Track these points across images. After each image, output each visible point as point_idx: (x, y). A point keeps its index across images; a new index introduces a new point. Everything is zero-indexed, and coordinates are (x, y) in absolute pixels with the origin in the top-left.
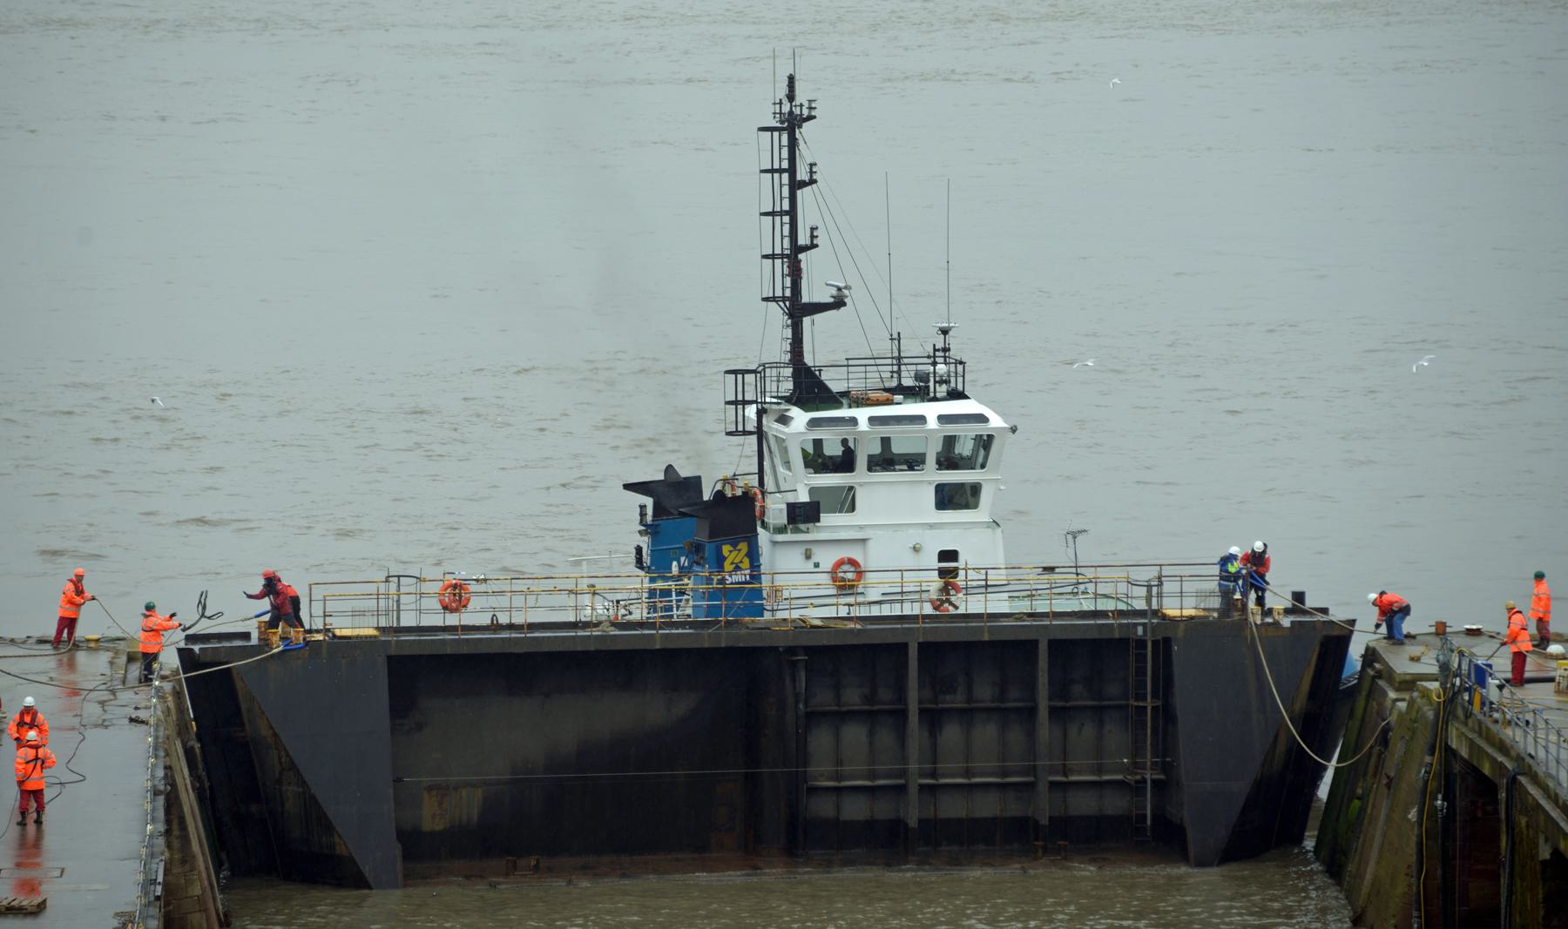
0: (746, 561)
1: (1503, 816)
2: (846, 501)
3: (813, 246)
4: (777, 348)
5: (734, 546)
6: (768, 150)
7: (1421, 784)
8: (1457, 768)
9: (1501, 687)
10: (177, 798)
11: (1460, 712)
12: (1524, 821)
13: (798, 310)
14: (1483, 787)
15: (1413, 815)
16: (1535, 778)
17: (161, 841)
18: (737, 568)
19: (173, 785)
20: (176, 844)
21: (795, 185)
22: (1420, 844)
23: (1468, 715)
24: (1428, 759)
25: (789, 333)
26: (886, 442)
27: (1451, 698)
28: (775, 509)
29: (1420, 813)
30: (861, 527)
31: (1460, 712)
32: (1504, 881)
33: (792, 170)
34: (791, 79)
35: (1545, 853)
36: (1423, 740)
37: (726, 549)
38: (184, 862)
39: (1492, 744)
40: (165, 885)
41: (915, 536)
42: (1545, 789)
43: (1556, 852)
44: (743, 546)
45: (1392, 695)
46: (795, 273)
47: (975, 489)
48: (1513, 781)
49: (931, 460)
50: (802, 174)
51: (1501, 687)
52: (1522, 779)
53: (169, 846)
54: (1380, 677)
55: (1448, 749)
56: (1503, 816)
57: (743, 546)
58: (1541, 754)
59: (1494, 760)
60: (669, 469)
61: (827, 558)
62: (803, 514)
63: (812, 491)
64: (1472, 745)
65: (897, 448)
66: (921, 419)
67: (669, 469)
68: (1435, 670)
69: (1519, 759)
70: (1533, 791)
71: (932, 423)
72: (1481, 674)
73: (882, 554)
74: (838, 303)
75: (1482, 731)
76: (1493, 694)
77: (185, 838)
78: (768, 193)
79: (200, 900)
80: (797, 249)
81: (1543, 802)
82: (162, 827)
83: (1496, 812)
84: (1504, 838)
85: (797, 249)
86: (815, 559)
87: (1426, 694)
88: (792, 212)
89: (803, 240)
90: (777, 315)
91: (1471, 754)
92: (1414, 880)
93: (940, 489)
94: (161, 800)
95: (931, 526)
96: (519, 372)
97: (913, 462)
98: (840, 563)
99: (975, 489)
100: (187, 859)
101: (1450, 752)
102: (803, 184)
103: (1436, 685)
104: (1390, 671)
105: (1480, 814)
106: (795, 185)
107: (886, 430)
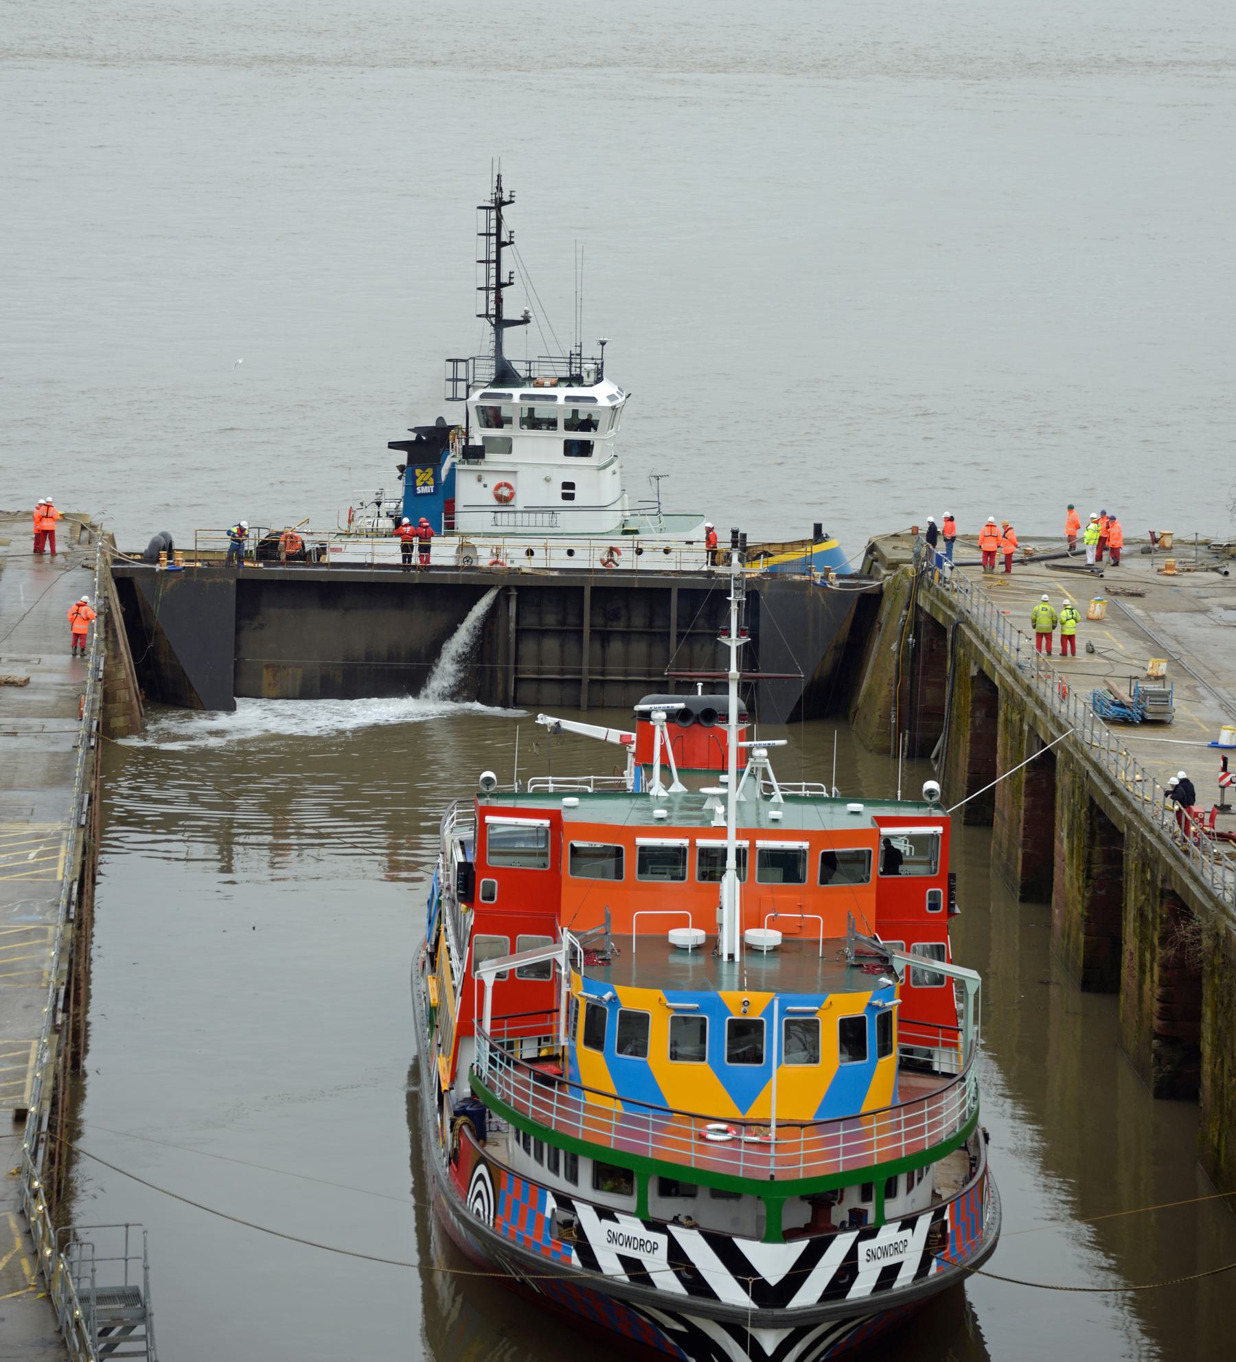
0: (432, 480)
1: (949, 648)
2: (506, 446)
3: (511, 284)
4: (488, 348)
5: (424, 469)
6: (482, 221)
7: (899, 628)
8: (922, 618)
9: (952, 568)
10: (112, 617)
11: (926, 584)
12: (962, 652)
13: (500, 323)
14: (939, 630)
15: (894, 647)
17: (102, 646)
18: (425, 484)
19: (109, 608)
20: (110, 646)
21: (500, 244)
22: (898, 665)
23: (931, 585)
24: (904, 612)
25: (493, 338)
26: (531, 410)
27: (920, 576)
29: (899, 645)
30: (515, 464)
31: (926, 584)
32: (948, 690)
33: (498, 235)
34: (499, 176)
35: (974, 672)
36: (902, 601)
37: (418, 472)
38: (115, 657)
39: (945, 604)
40: (105, 671)
41: (547, 472)
42: (976, 632)
43: (981, 671)
44: (430, 471)
45: (884, 572)
46: (499, 301)
48: (957, 627)
49: (561, 424)
50: (504, 238)
51: (952, 568)
52: (962, 626)
53: (107, 647)
54: (876, 560)
55: (917, 606)
56: (949, 648)
57: (430, 471)
58: (975, 611)
59: (945, 614)
60: (440, 419)
61: (492, 481)
63: (484, 439)
64: (932, 603)
65: (537, 415)
67: (440, 419)
68: (910, 556)
69: (961, 613)
70: (969, 633)
71: (561, 401)
74: (526, 321)
75: (939, 595)
76: (947, 573)
77: (116, 642)
78: (482, 248)
79: (125, 682)
80: (500, 285)
81: (975, 641)
82: (103, 636)
83: (945, 646)
84: (949, 662)
85: (500, 285)
86: (484, 482)
87: (905, 572)
88: (498, 261)
89: (504, 279)
90: (487, 327)
91: (931, 610)
92: (893, 688)
93: (566, 442)
94: (102, 618)
95: (560, 466)
97: (552, 424)
98: (499, 487)
100: (116, 655)
101: (918, 609)
102: (505, 244)
104: (883, 556)
105: (935, 647)
106: (500, 244)
107: (532, 404)
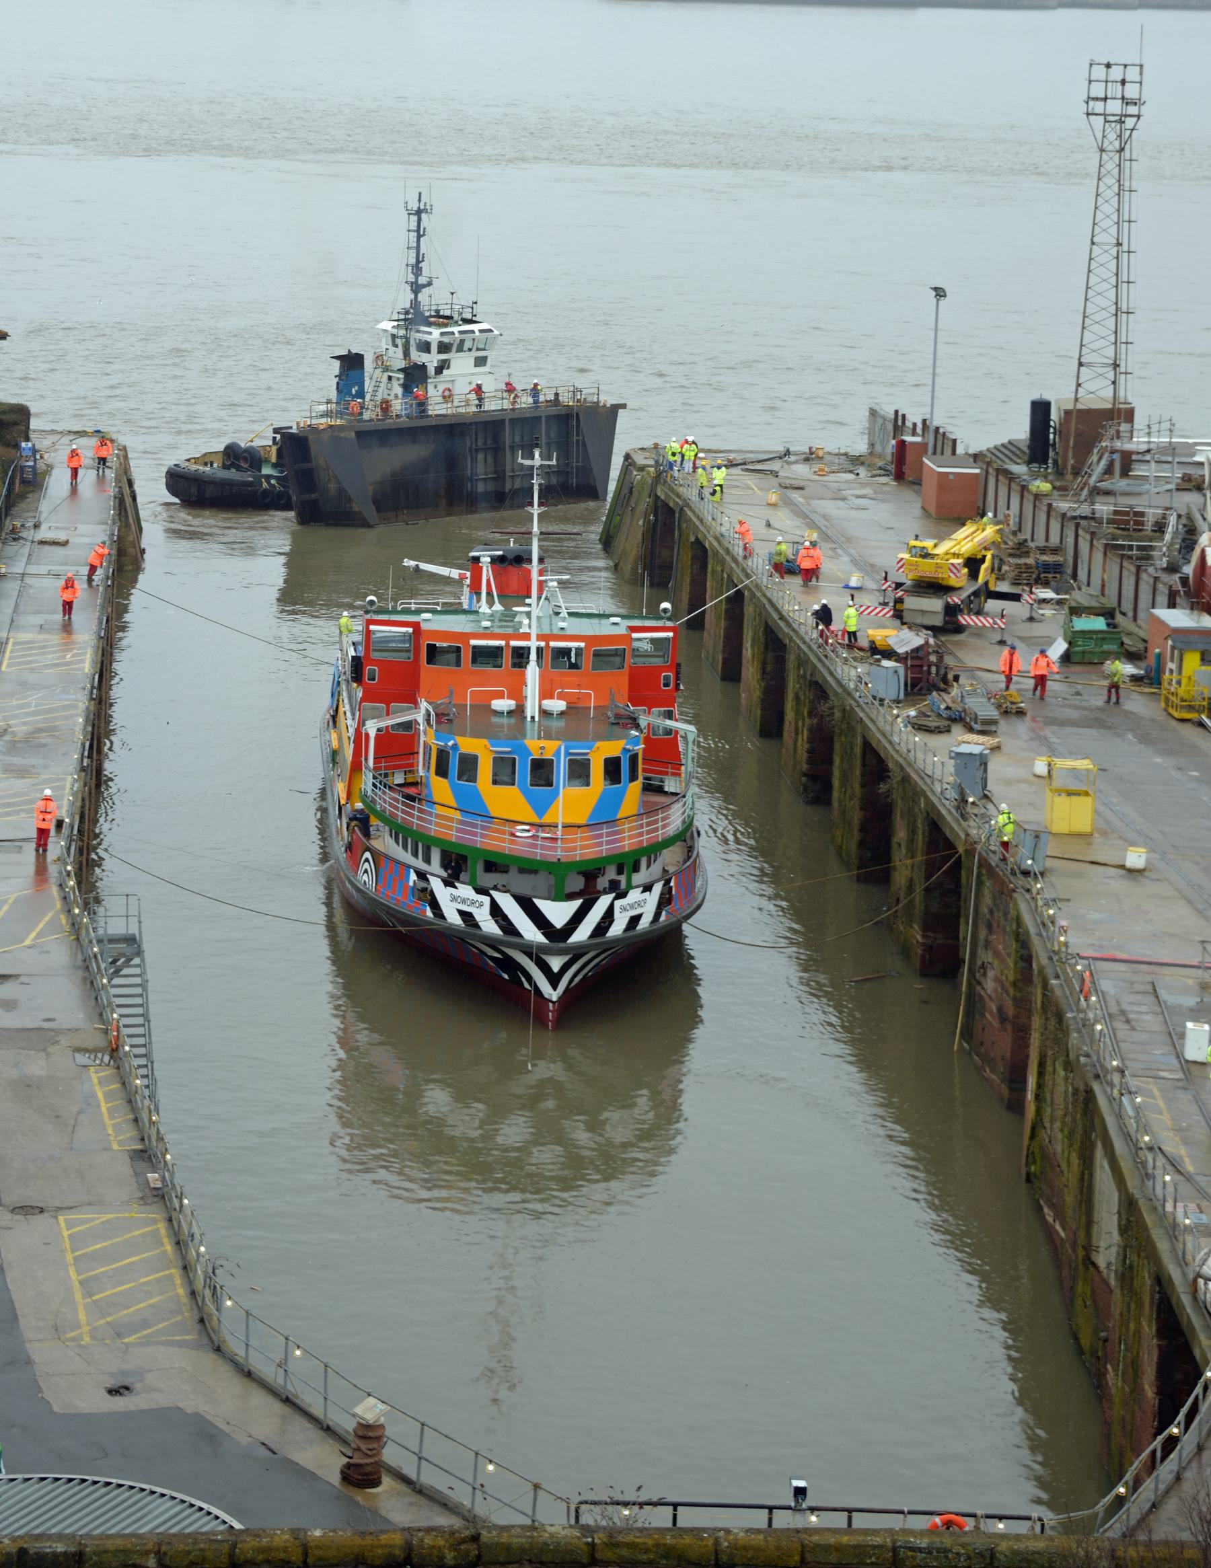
15: (641, 522)
16: (690, 508)
23: (665, 482)
27: (659, 475)
28: (431, 370)
35: (692, 539)
36: (646, 493)
42: (694, 512)
47: (486, 358)
48: (682, 509)
62: (439, 370)
66: (473, 332)
70: (689, 513)
72: (671, 465)
73: (459, 388)
77: (127, 517)
87: (649, 473)
93: (477, 359)
96: (335, 722)
99: (486, 358)
101: (657, 497)
103: (652, 469)
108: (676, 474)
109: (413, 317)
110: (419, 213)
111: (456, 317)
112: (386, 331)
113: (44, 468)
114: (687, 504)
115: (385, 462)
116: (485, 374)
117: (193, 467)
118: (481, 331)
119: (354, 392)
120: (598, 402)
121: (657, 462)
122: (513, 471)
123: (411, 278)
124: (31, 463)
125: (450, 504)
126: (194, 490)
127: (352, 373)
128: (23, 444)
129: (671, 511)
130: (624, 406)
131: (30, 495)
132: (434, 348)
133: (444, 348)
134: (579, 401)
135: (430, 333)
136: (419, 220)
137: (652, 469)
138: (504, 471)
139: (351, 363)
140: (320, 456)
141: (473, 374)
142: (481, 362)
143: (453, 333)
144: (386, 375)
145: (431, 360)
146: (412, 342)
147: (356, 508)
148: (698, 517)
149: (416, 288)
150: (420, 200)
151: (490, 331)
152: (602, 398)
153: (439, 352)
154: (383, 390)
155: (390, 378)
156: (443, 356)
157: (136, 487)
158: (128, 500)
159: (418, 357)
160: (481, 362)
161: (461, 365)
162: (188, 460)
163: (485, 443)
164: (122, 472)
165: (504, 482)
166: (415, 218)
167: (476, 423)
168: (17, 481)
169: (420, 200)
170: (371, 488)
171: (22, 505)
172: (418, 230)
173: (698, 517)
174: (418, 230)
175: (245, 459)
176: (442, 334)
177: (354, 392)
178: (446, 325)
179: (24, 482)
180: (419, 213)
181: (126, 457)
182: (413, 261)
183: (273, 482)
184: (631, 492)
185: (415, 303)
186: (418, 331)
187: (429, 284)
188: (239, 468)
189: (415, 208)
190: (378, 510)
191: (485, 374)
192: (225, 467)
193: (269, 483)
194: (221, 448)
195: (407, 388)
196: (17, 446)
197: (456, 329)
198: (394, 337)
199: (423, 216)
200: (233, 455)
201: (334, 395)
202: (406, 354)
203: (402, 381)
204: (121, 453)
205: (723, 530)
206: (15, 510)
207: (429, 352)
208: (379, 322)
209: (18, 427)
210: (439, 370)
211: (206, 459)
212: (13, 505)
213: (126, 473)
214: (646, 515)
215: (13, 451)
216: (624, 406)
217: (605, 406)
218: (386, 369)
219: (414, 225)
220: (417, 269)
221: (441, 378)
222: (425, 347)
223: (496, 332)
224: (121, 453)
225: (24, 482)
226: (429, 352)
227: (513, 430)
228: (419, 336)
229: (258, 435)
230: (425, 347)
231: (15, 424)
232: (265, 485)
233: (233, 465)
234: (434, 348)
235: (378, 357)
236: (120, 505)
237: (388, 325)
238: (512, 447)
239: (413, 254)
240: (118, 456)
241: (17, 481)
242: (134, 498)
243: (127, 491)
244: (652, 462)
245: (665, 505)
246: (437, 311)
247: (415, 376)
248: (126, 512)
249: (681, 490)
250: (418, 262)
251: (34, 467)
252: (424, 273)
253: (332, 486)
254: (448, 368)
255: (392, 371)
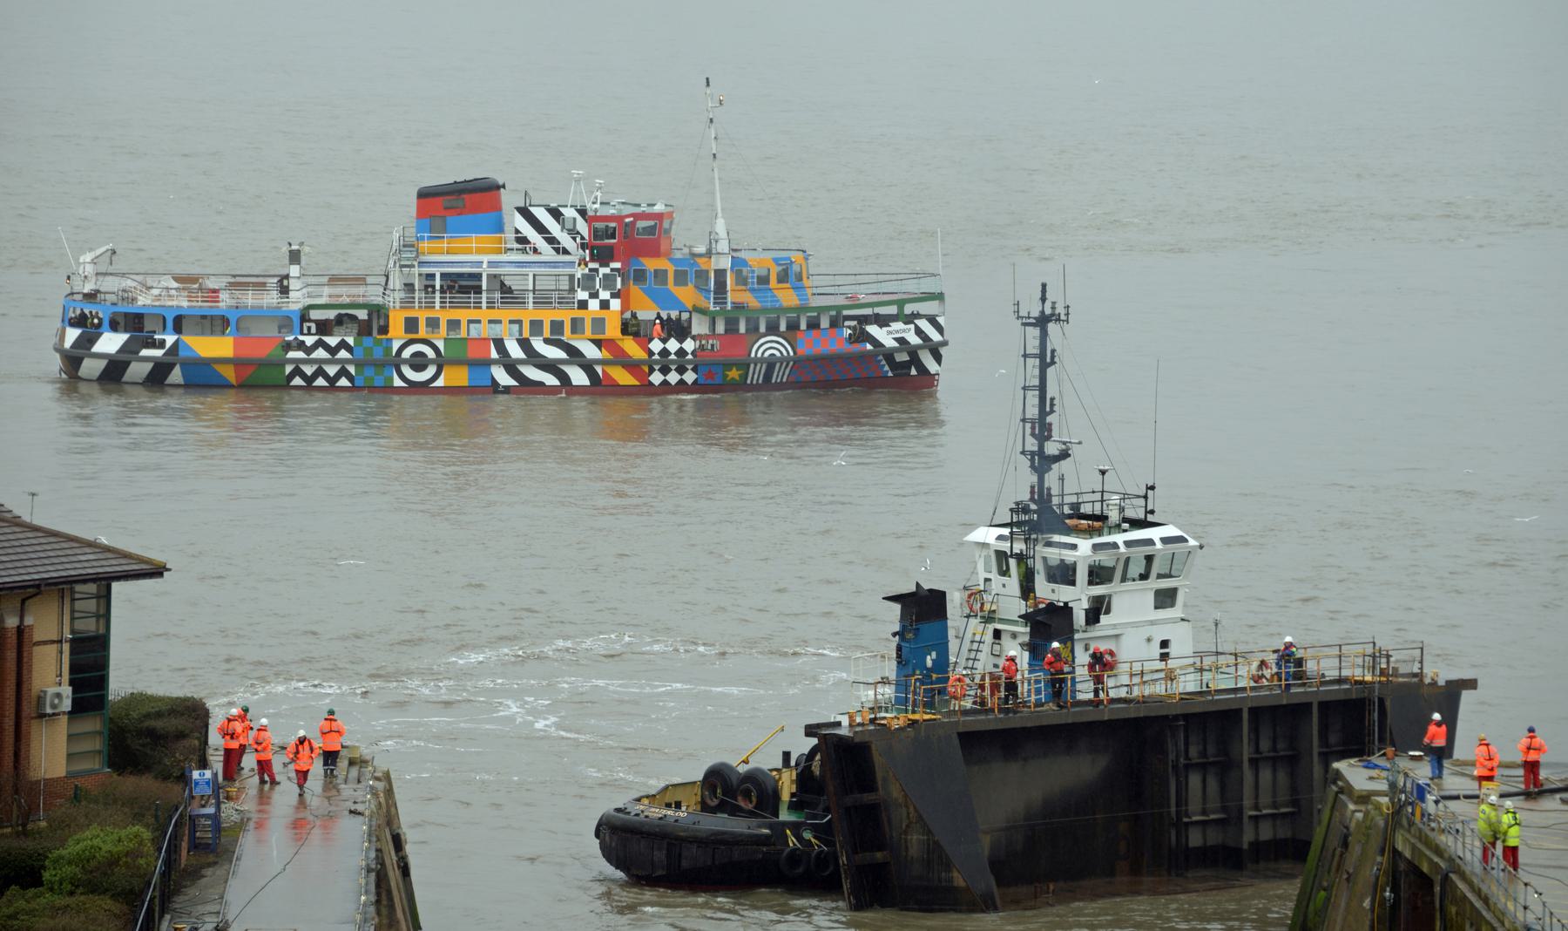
15: (1367, 903)
23: (1411, 824)
27: (1398, 810)
28: (1079, 617)
36: (1375, 843)
48: (1446, 878)
62: (1093, 616)
66: (1150, 542)
70: (1461, 885)
72: (1421, 792)
73: (1150, 649)
77: (391, 907)
87: (1378, 807)
101: (1396, 853)
103: (1385, 800)
108: (1430, 807)
109: (1038, 518)
110: (1042, 321)
111: (1114, 516)
112: (984, 545)
113: (236, 817)
114: (1455, 866)
115: (1012, 794)
116: (1173, 621)
117: (656, 812)
118: (1165, 540)
119: (929, 663)
120: (1420, 675)
121: (1393, 785)
122: (1256, 808)
123: (1032, 444)
124: (210, 810)
125: (1136, 870)
126: (660, 856)
127: (927, 628)
128: (196, 774)
129: (1425, 881)
130: (1471, 684)
131: (208, 872)
132: (1082, 575)
133: (1098, 575)
134: (1382, 672)
135: (1074, 547)
136: (1044, 335)
137: (1385, 800)
138: (1241, 810)
139: (923, 609)
140: (892, 787)
141: (1152, 623)
142: (1165, 598)
143: (1115, 546)
144: (991, 627)
145: (1078, 597)
146: (1039, 566)
147: (959, 881)
148: (1478, 893)
149: (1042, 462)
150: (1043, 299)
151: (1181, 539)
152: (1429, 672)
153: (1090, 583)
154: (984, 651)
155: (997, 634)
156: (1098, 590)
157: (409, 849)
158: (394, 875)
159: (1046, 591)
160: (1165, 598)
161: (1131, 605)
162: (639, 800)
163: (1203, 754)
164: (382, 821)
165: (1241, 830)
166: (1036, 332)
167: (1186, 717)
168: (184, 845)
169: (1043, 299)
170: (986, 841)
171: (192, 892)
172: (1042, 356)
173: (1478, 893)
174: (1042, 356)
175: (747, 795)
176: (1096, 547)
177: (929, 663)
178: (1100, 533)
179: (195, 846)
180: (1042, 321)
181: (389, 792)
182: (1032, 412)
183: (807, 835)
184: (1345, 844)
185: (1041, 496)
186: (1049, 544)
187: (1064, 455)
188: (735, 811)
189: (1036, 313)
190: (1000, 882)
191: (1173, 621)
192: (705, 807)
193: (799, 838)
194: (699, 776)
195: (1035, 649)
196: (184, 779)
197: (1119, 538)
198: (1001, 556)
199: (1051, 327)
200: (722, 786)
201: (890, 669)
202: (1027, 589)
203: (1027, 639)
204: (380, 785)
205: (1530, 918)
206: (179, 902)
207: (1073, 583)
208: (972, 526)
209: (186, 743)
210: (1093, 616)
211: (669, 796)
212: (177, 892)
213: (389, 823)
214: (1376, 889)
215: (177, 788)
216: (1471, 684)
217: (1434, 684)
218: (989, 618)
219: (1033, 346)
220: (1043, 431)
221: (1096, 631)
222: (1064, 573)
223: (1192, 542)
224: (380, 785)
225: (195, 846)
226: (1073, 583)
227: (1255, 730)
228: (1054, 554)
229: (769, 743)
230: (1064, 573)
231: (181, 736)
232: (792, 841)
233: (721, 807)
234: (1082, 575)
235: (973, 595)
236: (378, 886)
237: (988, 535)
238: (1254, 762)
239: (1033, 398)
240: (375, 794)
241: (184, 845)
242: (405, 871)
243: (391, 858)
244: (1384, 786)
245: (1415, 869)
246: (1075, 506)
247: (1049, 624)
248: (390, 899)
249: (1444, 840)
250: (1043, 413)
251: (216, 818)
252: (1055, 433)
253: (916, 841)
254: (1108, 612)
255: (1002, 621)
